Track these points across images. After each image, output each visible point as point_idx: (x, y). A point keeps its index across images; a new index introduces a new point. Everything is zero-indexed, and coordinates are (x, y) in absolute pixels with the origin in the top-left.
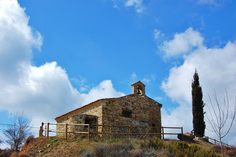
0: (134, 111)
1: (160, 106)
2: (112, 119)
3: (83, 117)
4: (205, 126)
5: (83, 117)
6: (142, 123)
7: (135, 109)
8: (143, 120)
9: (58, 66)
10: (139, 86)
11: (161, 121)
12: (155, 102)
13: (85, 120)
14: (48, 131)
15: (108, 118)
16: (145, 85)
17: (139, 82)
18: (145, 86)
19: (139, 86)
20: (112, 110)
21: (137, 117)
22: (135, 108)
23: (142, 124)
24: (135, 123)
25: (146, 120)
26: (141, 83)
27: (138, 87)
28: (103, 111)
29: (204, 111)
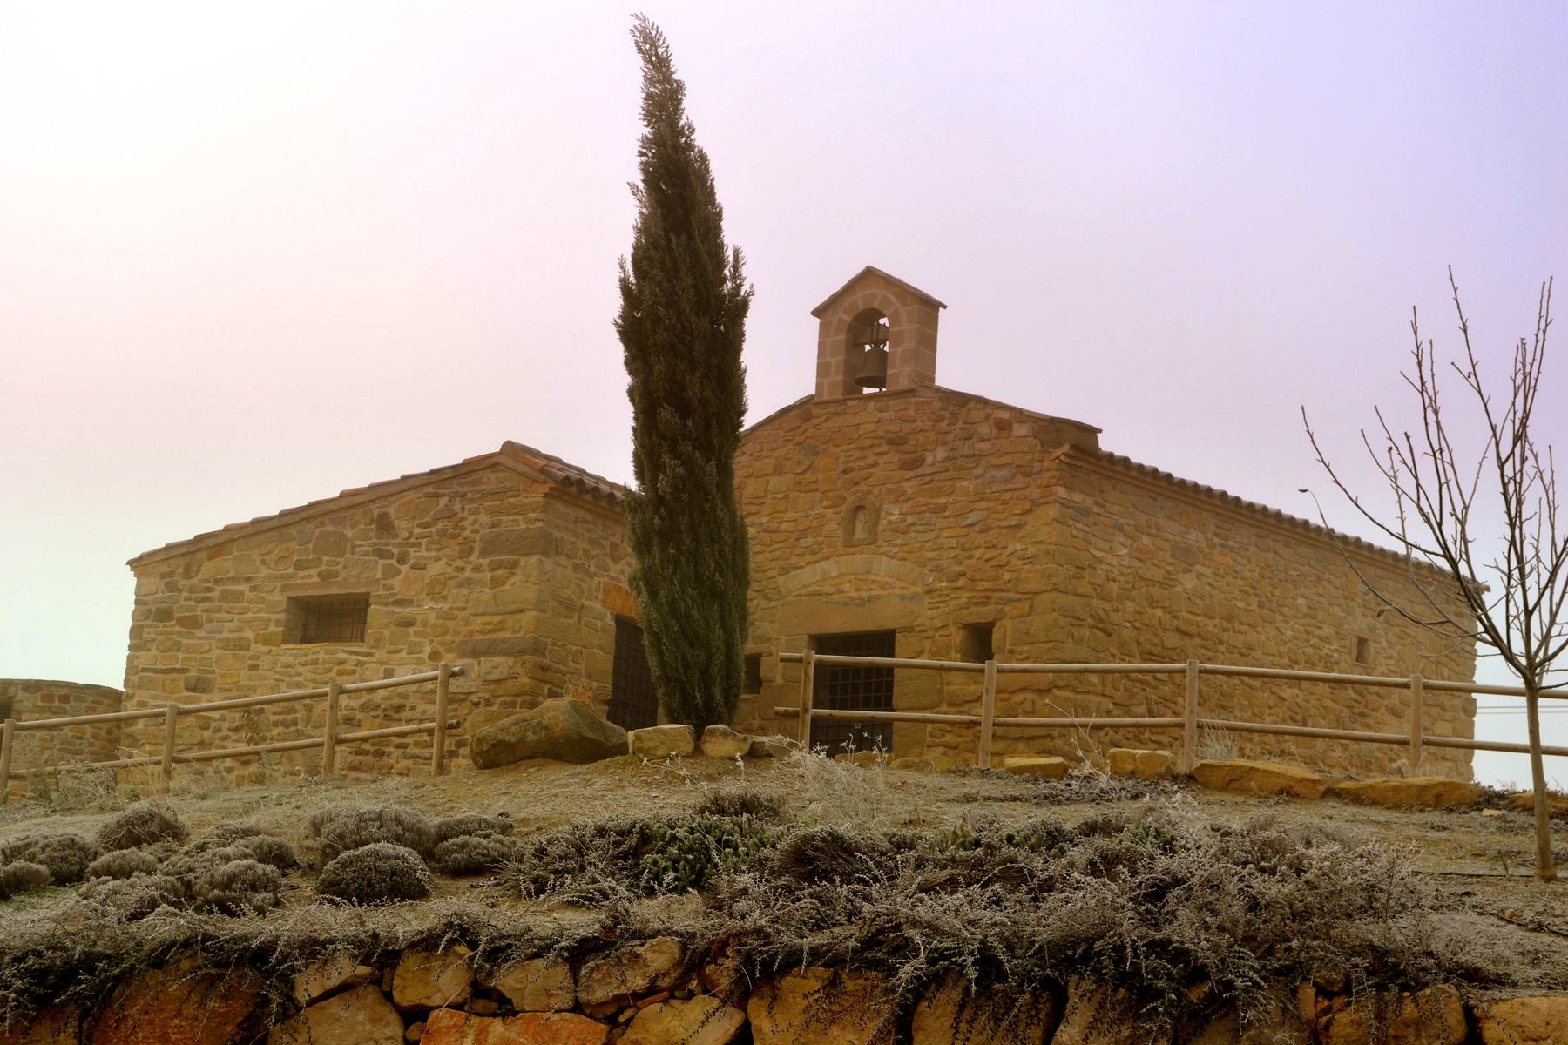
12: (1006, 415)
21: (1221, 643)
25: (508, 635)
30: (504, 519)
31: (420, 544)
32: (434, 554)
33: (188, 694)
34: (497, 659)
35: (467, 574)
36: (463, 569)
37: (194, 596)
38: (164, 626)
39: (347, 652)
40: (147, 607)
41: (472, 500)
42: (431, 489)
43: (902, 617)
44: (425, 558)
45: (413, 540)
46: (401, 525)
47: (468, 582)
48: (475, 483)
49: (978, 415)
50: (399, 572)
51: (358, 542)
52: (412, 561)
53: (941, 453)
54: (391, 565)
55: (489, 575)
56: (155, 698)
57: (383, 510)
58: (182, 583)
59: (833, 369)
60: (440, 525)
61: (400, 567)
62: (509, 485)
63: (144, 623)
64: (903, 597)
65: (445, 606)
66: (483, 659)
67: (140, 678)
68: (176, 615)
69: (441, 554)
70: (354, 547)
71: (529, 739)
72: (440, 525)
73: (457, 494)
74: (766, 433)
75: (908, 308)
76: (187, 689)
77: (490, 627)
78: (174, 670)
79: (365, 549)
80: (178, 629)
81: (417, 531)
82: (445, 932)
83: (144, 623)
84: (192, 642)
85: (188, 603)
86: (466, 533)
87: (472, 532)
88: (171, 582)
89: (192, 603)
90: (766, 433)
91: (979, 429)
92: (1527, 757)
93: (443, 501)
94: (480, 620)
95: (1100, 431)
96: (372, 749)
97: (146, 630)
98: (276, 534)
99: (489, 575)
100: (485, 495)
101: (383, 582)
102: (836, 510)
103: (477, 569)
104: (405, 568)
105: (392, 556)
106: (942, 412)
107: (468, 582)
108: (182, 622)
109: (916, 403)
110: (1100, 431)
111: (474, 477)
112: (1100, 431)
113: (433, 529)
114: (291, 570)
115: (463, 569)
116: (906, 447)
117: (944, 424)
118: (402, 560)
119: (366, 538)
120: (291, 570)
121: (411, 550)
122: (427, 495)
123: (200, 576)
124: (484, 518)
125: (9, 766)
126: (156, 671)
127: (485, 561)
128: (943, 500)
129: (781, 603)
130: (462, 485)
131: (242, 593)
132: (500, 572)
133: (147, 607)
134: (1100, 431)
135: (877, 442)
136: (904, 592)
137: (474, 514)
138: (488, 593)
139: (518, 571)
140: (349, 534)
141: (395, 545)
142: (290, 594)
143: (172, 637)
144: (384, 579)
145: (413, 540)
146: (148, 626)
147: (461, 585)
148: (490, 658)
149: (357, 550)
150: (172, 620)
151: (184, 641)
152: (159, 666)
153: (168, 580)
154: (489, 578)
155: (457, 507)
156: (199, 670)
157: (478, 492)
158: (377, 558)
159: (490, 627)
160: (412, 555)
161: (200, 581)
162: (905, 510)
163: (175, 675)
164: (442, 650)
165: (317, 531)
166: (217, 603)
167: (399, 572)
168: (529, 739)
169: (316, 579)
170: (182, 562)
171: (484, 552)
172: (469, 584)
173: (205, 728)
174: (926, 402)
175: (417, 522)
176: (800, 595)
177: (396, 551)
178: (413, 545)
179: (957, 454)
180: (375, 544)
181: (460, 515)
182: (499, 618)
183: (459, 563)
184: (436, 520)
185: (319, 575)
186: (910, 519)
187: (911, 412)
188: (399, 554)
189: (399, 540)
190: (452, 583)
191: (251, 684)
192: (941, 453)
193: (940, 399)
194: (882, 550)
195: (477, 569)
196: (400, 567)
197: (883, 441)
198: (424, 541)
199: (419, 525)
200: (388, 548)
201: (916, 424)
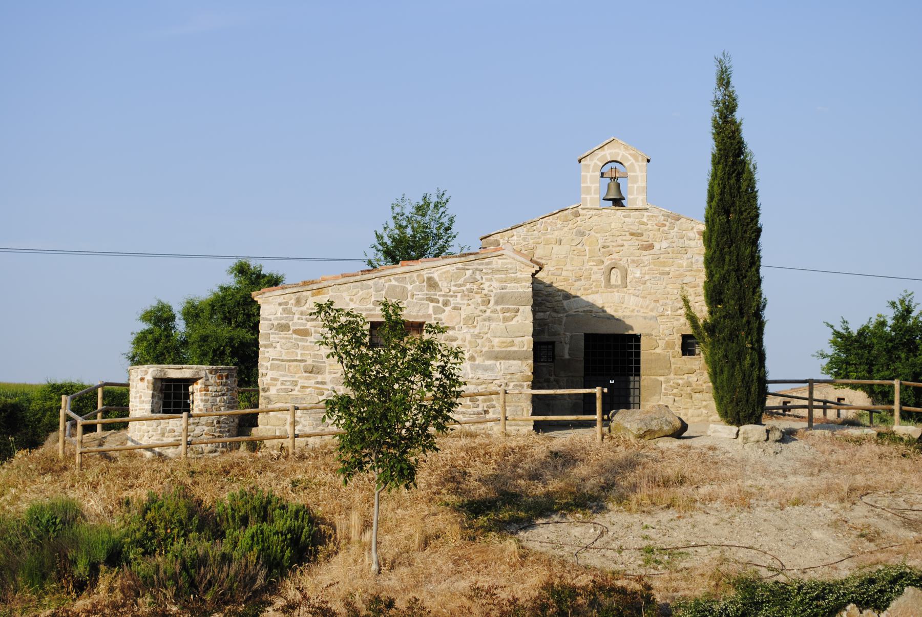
30: (509, 285)
31: (456, 296)
32: (466, 302)
34: (511, 362)
35: (488, 313)
36: (485, 311)
38: (286, 334)
40: (270, 322)
41: (486, 274)
42: (460, 265)
43: (645, 328)
44: (461, 304)
45: (451, 293)
46: (443, 285)
47: (489, 319)
48: (488, 264)
50: (444, 311)
51: (415, 293)
52: (452, 305)
53: (665, 244)
54: (438, 307)
55: (501, 316)
56: (283, 376)
57: (430, 275)
58: (294, 309)
59: (593, 191)
60: (468, 286)
61: (445, 308)
62: (510, 266)
63: (270, 332)
64: (645, 318)
65: (477, 331)
66: (502, 362)
67: (271, 364)
68: (292, 328)
69: (470, 302)
71: (665, 429)
72: (468, 286)
73: (477, 269)
74: (549, 221)
75: (640, 164)
77: (505, 344)
78: (296, 361)
79: (420, 296)
80: (295, 336)
81: (453, 288)
83: (270, 332)
84: (306, 344)
85: (300, 321)
86: (485, 292)
87: (489, 291)
88: (286, 308)
89: (304, 321)
90: (549, 221)
91: (688, 234)
93: (469, 273)
97: (271, 336)
98: (358, 284)
99: (501, 316)
100: (494, 271)
102: (600, 267)
103: (495, 311)
104: (447, 309)
105: (438, 302)
106: (664, 222)
107: (489, 319)
108: (296, 332)
109: (648, 216)
111: (487, 260)
113: (464, 288)
114: (371, 306)
115: (485, 311)
116: (643, 238)
117: (666, 228)
118: (446, 304)
119: (421, 290)
120: (371, 306)
121: (451, 299)
122: (457, 269)
123: (307, 305)
124: (495, 284)
125: (294, 430)
126: (282, 361)
127: (499, 308)
128: (667, 269)
129: (565, 314)
130: (480, 264)
132: (508, 315)
133: (270, 322)
135: (624, 233)
136: (646, 315)
137: (489, 281)
138: (502, 325)
139: (519, 314)
140: (409, 287)
143: (291, 340)
144: (435, 314)
145: (451, 293)
146: (272, 333)
147: (485, 320)
148: (507, 361)
149: (415, 297)
150: (289, 331)
151: (300, 344)
152: (284, 357)
153: (285, 307)
154: (501, 318)
155: (478, 277)
157: (490, 269)
158: (428, 302)
159: (505, 344)
160: (452, 302)
161: (307, 308)
162: (643, 272)
163: (295, 363)
164: (476, 355)
165: (387, 285)
167: (444, 311)
168: (665, 429)
170: (294, 297)
171: (497, 303)
172: (489, 320)
174: (655, 216)
175: (453, 283)
176: (578, 311)
177: (441, 299)
178: (452, 296)
179: (674, 245)
180: (427, 294)
181: (480, 281)
182: (511, 339)
183: (483, 308)
184: (465, 283)
186: (647, 277)
187: (645, 220)
188: (444, 301)
189: (442, 293)
190: (479, 318)
192: (665, 244)
194: (630, 291)
195: (495, 311)
196: (445, 308)
197: (627, 234)
198: (459, 295)
199: (455, 285)
200: (435, 297)
201: (648, 226)
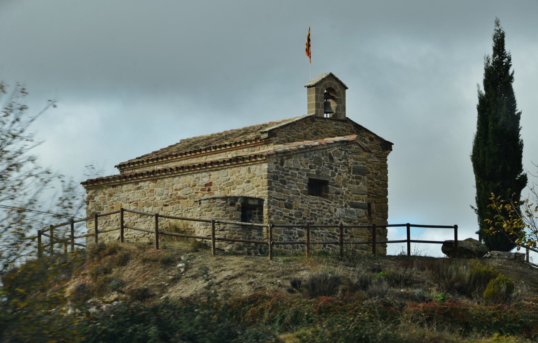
0: (335, 178)
1: (387, 150)
2: (287, 201)
3: (238, 203)
4: (443, 252)
5: (238, 203)
6: (352, 209)
7: (337, 174)
8: (354, 201)
9: (464, 337)
10: (330, 90)
11: (387, 194)
12: (373, 136)
13: (240, 209)
14: (123, 228)
15: (279, 200)
16: (347, 86)
17: (331, 76)
18: (347, 88)
19: (330, 90)
20: (287, 181)
21: (339, 194)
22: (336, 171)
23: (352, 213)
24: (335, 210)
25: (360, 202)
26: (337, 79)
27: (325, 91)
28: (269, 183)
29: (520, 134)
33: (286, 209)
37: (284, 172)
39: (325, 201)
49: (365, 134)
67: (273, 201)
70: (324, 163)
76: (286, 207)
82: (350, 310)
92: (411, 239)
94: (355, 195)
95: (393, 144)
96: (332, 235)
101: (332, 178)
110: (393, 144)
112: (393, 144)
131: (296, 174)
134: (393, 144)
141: (334, 165)
142: (309, 177)
150: (278, 180)
156: (288, 201)
166: (290, 177)
169: (315, 173)
173: (290, 222)
185: (316, 172)
190: (347, 181)
191: (303, 208)
193: (354, 126)
